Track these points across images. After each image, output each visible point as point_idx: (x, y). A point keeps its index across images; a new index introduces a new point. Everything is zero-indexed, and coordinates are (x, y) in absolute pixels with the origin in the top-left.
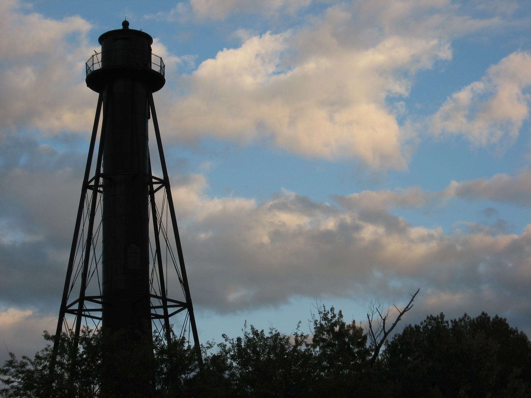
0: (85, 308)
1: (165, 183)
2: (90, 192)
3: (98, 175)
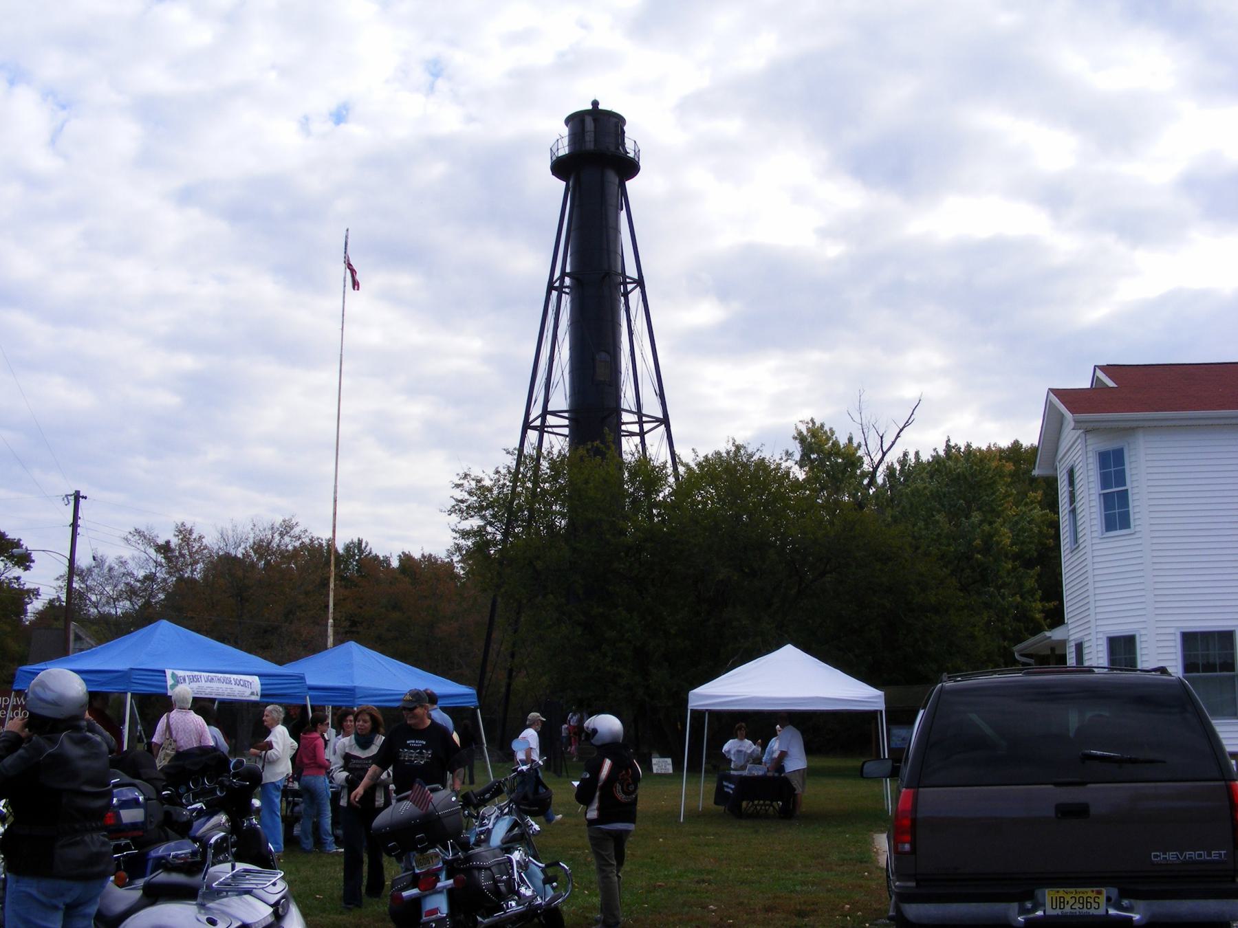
1: (640, 282)
2: (554, 293)
3: (563, 274)
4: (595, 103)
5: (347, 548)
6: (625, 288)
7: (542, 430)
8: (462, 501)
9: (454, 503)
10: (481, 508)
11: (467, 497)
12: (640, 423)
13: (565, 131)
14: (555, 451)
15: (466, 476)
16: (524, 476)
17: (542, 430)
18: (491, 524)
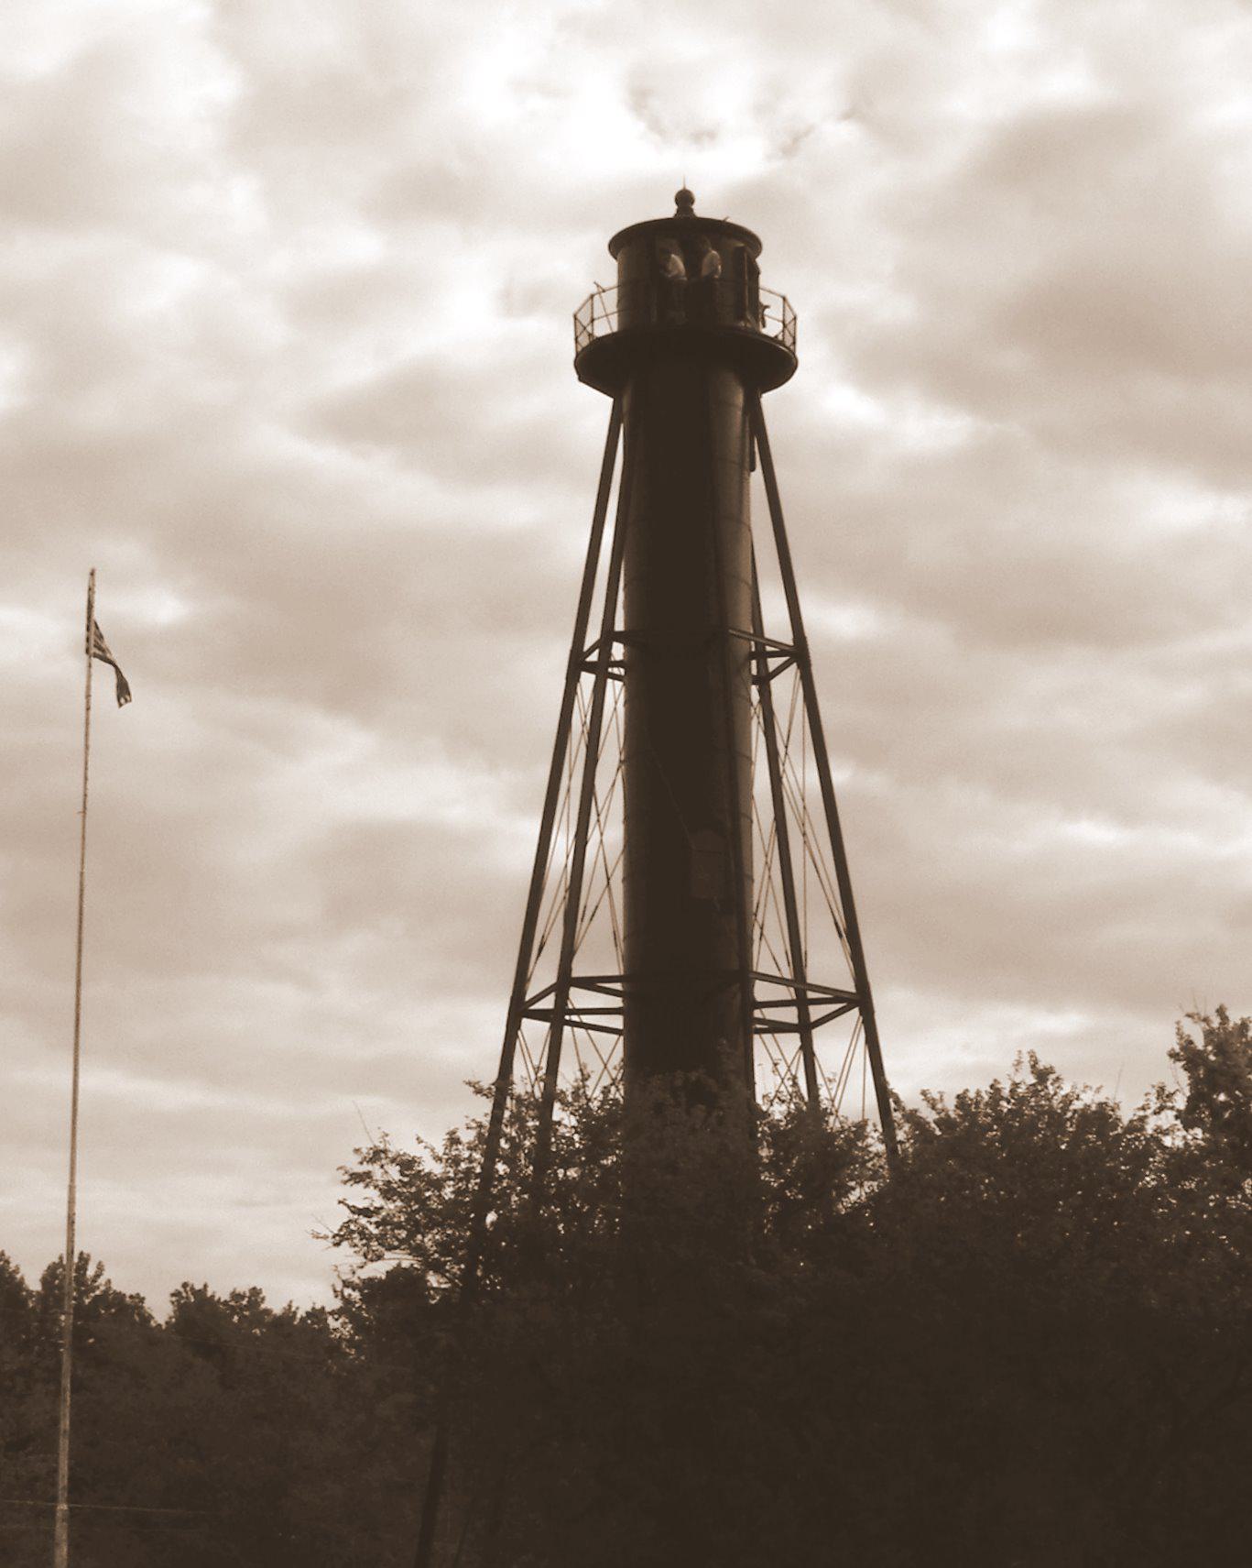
2: (588, 680)
3: (608, 635)
4: (684, 199)
5: (52, 1276)
6: (762, 665)
7: (558, 1018)
8: (366, 1212)
9: (346, 1215)
10: (415, 1228)
11: (379, 1202)
12: (802, 1003)
13: (609, 271)
14: (594, 1092)
15: (377, 1155)
16: (516, 1146)
17: (558, 1018)
18: (438, 1268)
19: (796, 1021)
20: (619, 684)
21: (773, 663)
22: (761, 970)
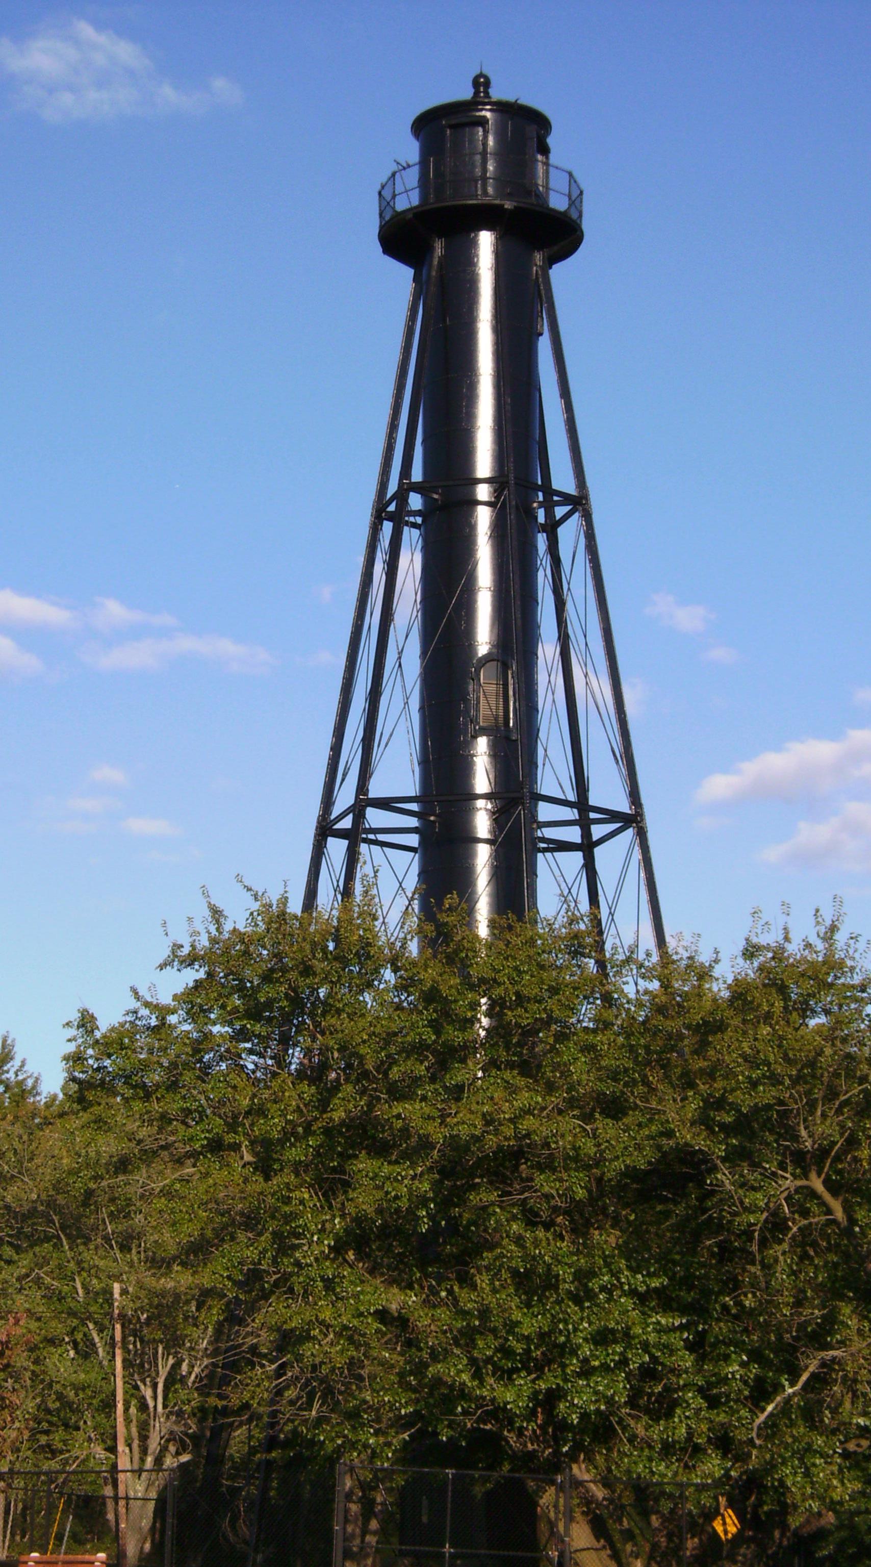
0: (367, 826)
1: (579, 502)
2: (388, 527)
6: (549, 514)
7: (355, 837)
12: (584, 824)
13: (411, 150)
17: (355, 837)
19: (579, 841)
20: (416, 533)
21: (560, 512)
22: (544, 792)
